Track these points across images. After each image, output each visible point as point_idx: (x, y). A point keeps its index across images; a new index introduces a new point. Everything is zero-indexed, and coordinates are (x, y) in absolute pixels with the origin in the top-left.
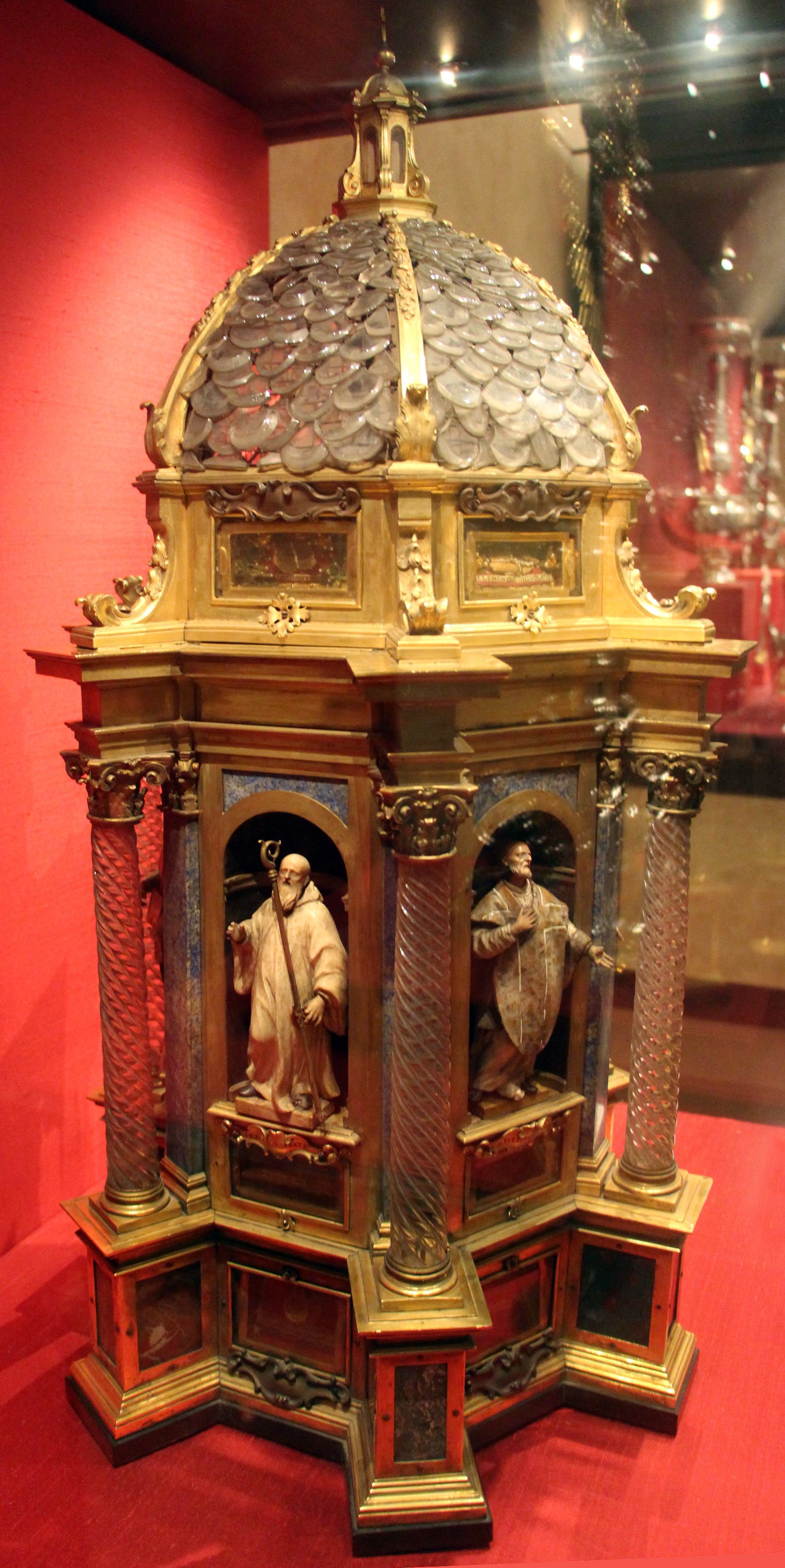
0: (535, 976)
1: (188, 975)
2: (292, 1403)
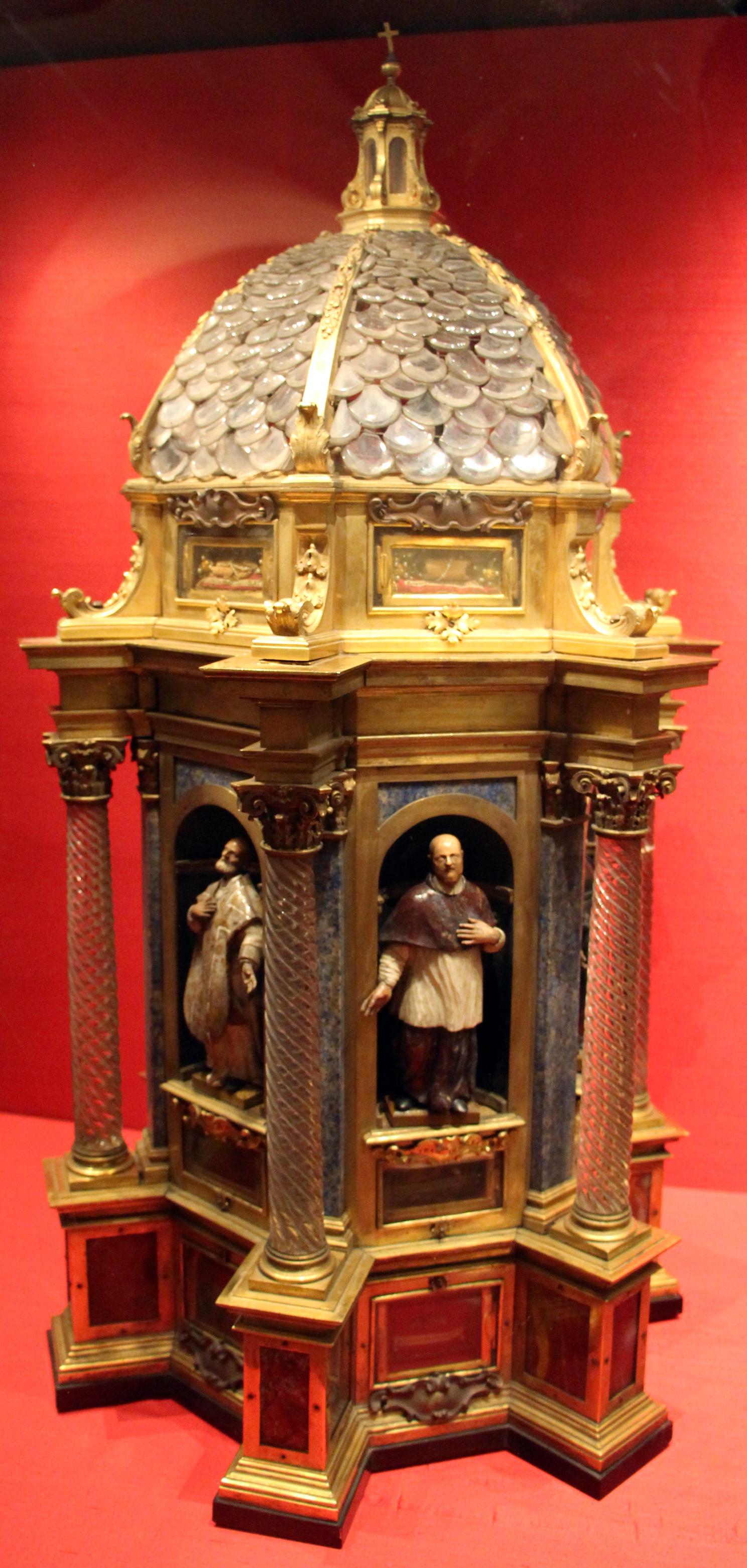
2: (450, 1414)
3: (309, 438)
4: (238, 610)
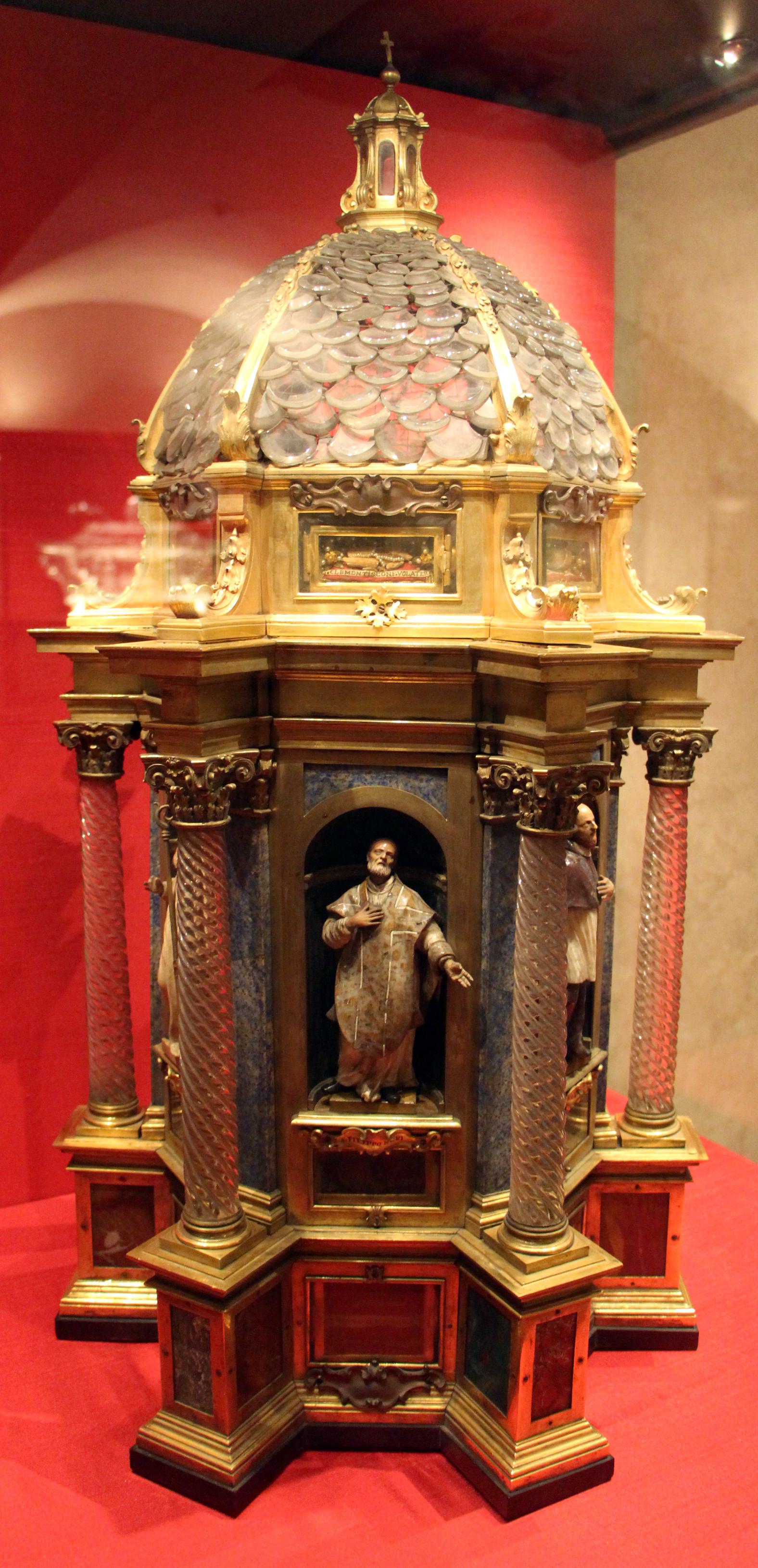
0: (376, 976)
1: (151, 922)
3: (525, 430)
4: (403, 602)
